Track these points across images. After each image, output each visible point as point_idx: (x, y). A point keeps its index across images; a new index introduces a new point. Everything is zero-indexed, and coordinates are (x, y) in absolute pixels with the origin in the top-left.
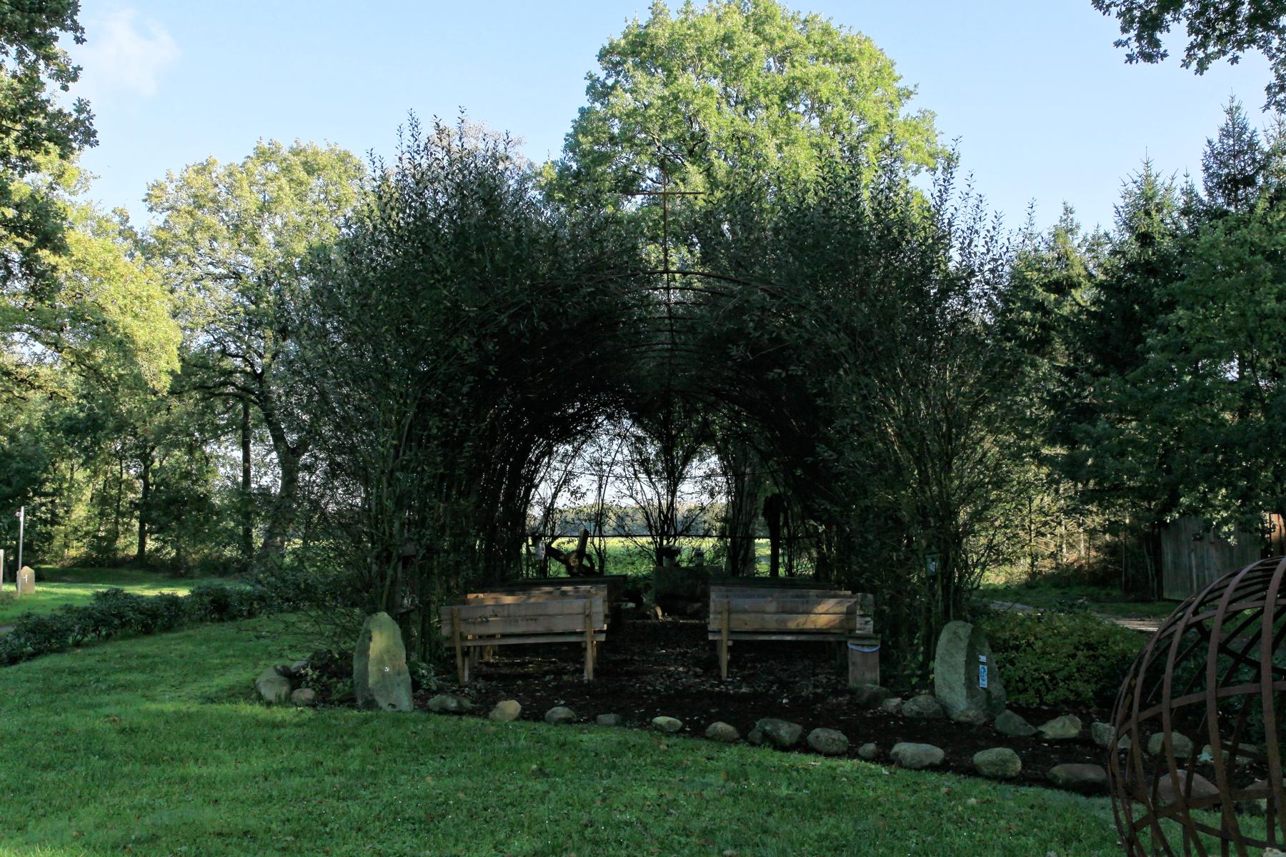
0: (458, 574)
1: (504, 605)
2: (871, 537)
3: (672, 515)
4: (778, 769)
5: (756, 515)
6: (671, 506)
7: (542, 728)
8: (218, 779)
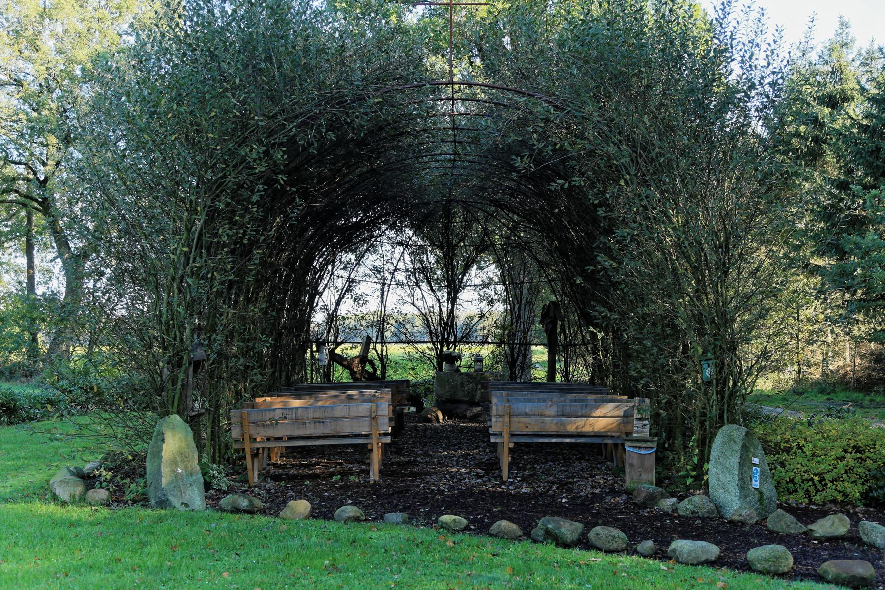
0: (246, 379)
1: (292, 408)
2: (649, 344)
3: (452, 322)
4: (560, 564)
5: (533, 322)
6: (451, 313)
7: (332, 526)
8: (20, 575)
